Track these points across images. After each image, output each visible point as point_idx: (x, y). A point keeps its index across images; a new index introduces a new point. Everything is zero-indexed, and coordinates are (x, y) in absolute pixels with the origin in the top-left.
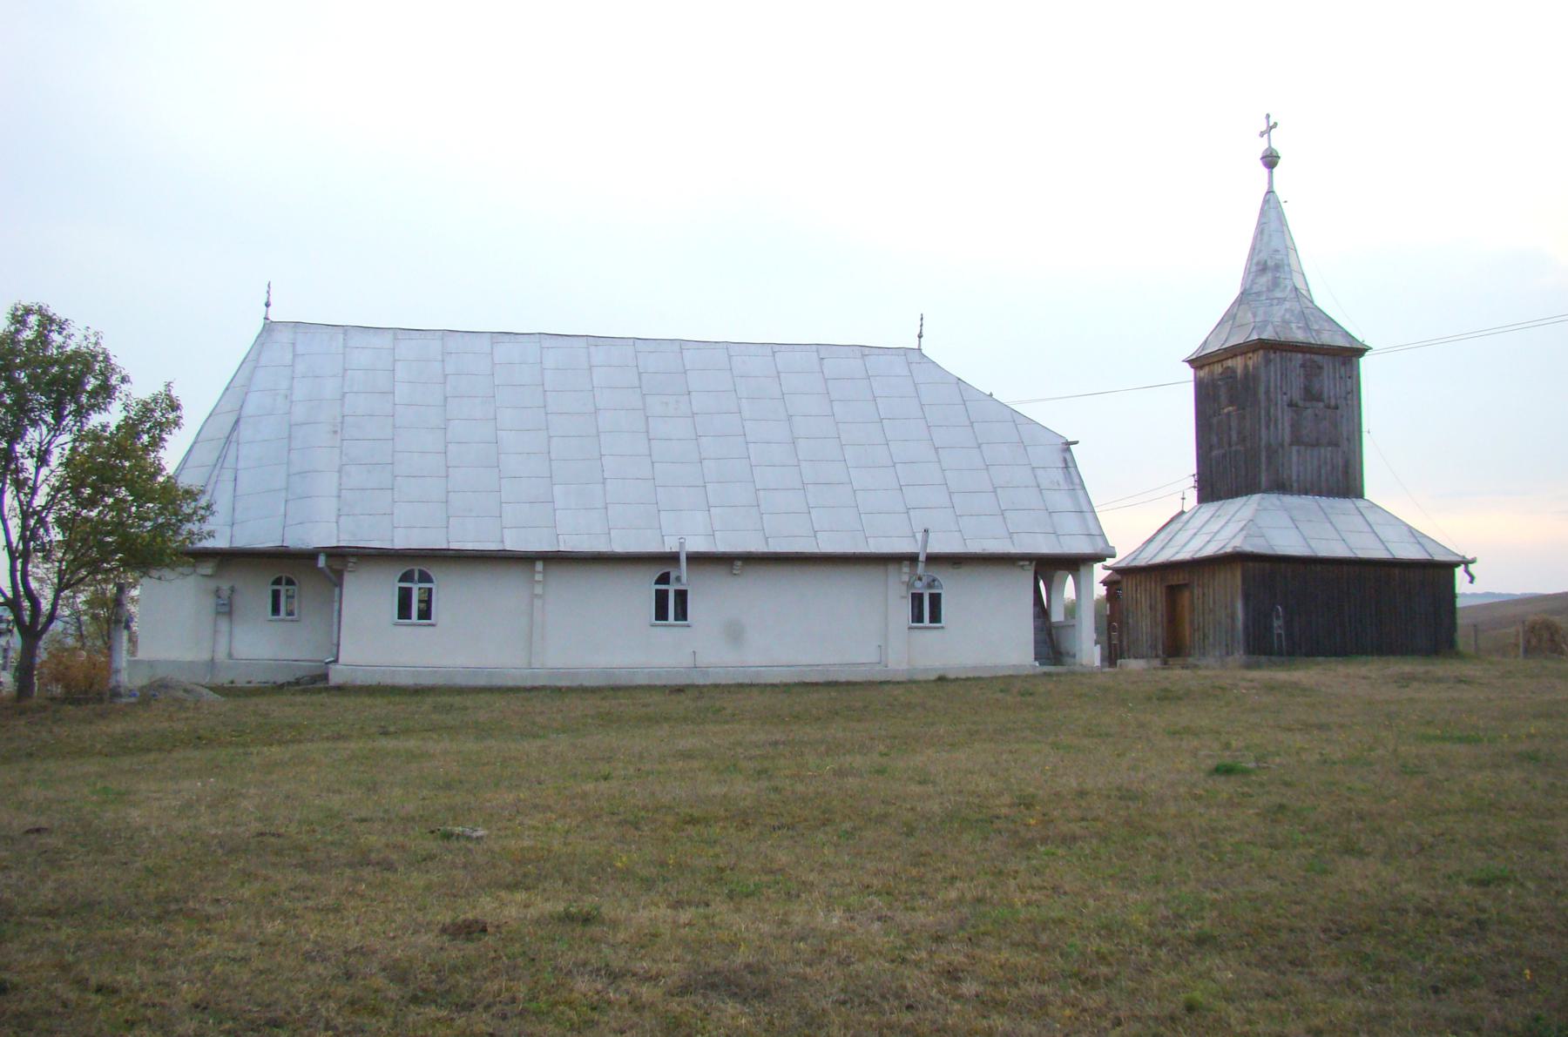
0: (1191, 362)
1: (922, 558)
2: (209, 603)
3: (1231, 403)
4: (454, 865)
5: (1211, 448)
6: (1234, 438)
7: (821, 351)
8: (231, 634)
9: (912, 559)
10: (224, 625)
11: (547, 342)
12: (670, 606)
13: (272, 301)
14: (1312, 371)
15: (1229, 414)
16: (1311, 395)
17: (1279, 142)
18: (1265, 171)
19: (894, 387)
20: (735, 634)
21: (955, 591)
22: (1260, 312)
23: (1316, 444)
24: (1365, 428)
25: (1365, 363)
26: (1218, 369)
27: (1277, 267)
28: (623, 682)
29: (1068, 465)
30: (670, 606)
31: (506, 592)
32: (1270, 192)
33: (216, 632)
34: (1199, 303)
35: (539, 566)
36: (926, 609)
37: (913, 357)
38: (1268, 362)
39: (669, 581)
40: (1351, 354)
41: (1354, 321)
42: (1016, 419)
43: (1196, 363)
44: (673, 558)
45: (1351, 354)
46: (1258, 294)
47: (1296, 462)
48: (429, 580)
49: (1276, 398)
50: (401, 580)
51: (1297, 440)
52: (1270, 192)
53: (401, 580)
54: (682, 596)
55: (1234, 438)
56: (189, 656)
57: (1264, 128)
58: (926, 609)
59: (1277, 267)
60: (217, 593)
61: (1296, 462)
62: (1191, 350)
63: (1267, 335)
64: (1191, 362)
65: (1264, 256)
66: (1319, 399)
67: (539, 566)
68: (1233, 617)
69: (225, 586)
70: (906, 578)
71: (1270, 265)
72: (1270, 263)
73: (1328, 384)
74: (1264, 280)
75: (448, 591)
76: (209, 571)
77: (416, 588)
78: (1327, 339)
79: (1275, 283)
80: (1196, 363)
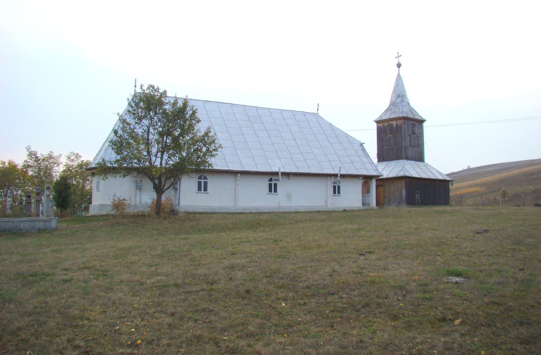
1: (339, 175)
2: (134, 185)
3: (391, 134)
5: (383, 147)
6: (392, 143)
7: (270, 110)
8: (141, 196)
9: (336, 175)
10: (138, 193)
11: (220, 105)
12: (273, 188)
14: (414, 125)
15: (390, 137)
16: (414, 133)
17: (401, 60)
18: (398, 68)
19: (309, 124)
20: (289, 197)
21: (345, 186)
22: (400, 108)
23: (414, 147)
24: (425, 142)
25: (424, 124)
26: (386, 124)
27: (403, 96)
28: (261, 211)
29: (364, 150)
30: (273, 188)
31: (228, 183)
32: (399, 74)
33: (136, 195)
34: (379, 106)
35: (239, 175)
36: (336, 190)
37: (316, 115)
38: (404, 123)
39: (273, 180)
40: (422, 121)
41: (422, 113)
42: (347, 136)
43: (378, 122)
44: (276, 174)
45: (422, 121)
46: (398, 103)
47: (411, 152)
49: (400, 134)
51: (410, 146)
52: (399, 74)
54: (275, 185)
55: (392, 143)
57: (397, 56)
58: (336, 190)
59: (403, 96)
60: (136, 182)
61: (411, 152)
62: (377, 117)
63: (404, 115)
64: (376, 122)
65: (399, 92)
66: (415, 134)
67: (239, 175)
68: (401, 194)
69: (138, 180)
70: (333, 181)
71: (399, 96)
72: (401, 95)
73: (416, 130)
74: (399, 100)
75: (283, 186)
76: (135, 175)
77: (203, 181)
79: (402, 101)
80: (378, 122)
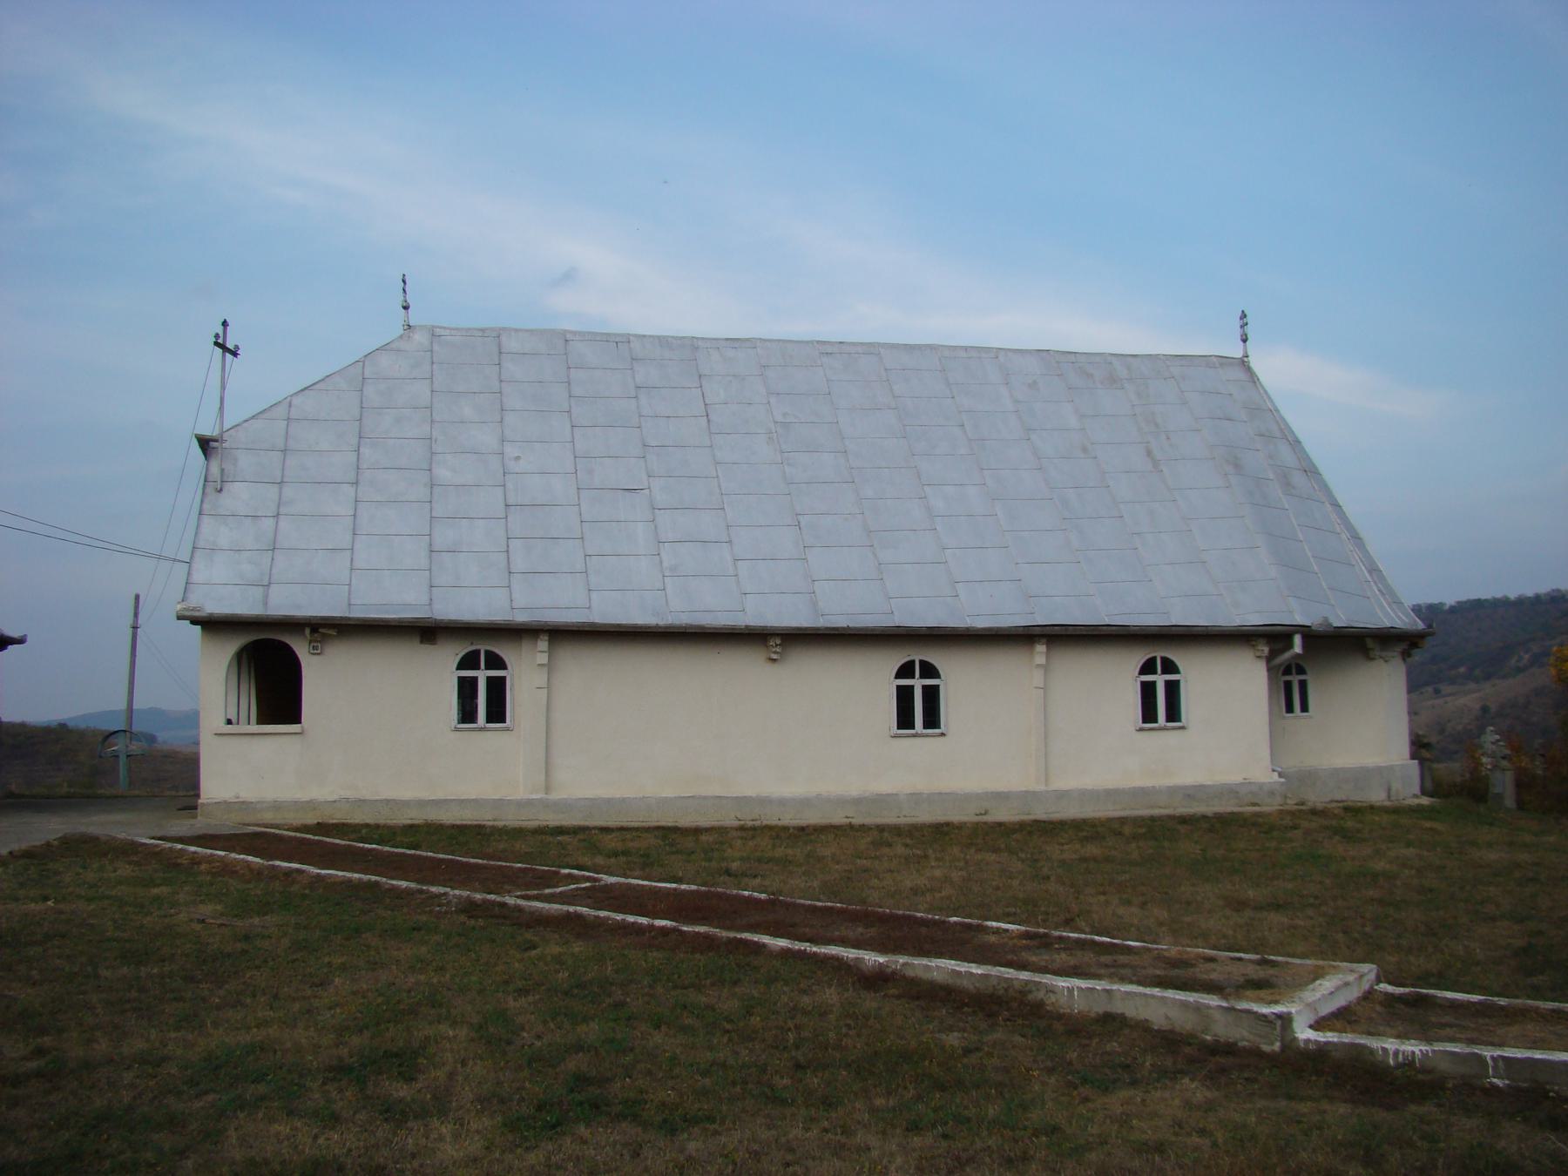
36: (918, 709)
53: (899, 675)
67: (543, 644)
77: (1160, 680)
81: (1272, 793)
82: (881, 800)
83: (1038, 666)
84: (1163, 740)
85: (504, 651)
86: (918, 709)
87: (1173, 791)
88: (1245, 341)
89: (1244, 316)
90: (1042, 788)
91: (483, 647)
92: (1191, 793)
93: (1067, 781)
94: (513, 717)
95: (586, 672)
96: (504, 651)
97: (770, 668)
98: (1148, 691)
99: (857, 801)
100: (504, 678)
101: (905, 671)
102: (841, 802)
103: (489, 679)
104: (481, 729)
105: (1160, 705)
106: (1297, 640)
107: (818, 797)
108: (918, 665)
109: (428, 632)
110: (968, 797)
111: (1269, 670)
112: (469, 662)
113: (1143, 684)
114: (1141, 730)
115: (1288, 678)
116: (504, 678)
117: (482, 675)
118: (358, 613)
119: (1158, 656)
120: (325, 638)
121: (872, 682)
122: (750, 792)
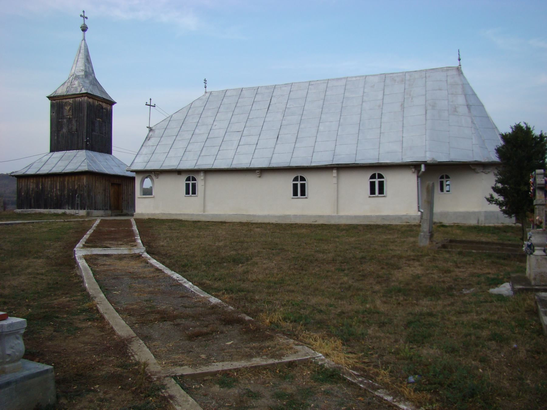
0: (49, 98)
4: (279, 309)
13: (461, 57)
21: (392, 181)
26: (96, 103)
36: (300, 190)
40: (112, 103)
45: (112, 103)
48: (383, 177)
50: (294, 180)
53: (294, 180)
56: (476, 210)
62: (50, 93)
64: (49, 98)
67: (202, 174)
77: (377, 181)
78: (97, 93)
81: (415, 219)
82: (285, 217)
83: (334, 177)
84: (378, 200)
85: (305, 175)
86: (300, 190)
87: (378, 217)
88: (205, 87)
89: (205, 80)
90: (335, 214)
91: (377, 172)
92: (384, 218)
93: (341, 213)
94: (386, 192)
95: (214, 182)
96: (305, 175)
97: (259, 179)
98: (187, 186)
99: (279, 217)
100: (383, 182)
101: (296, 179)
102: (275, 217)
103: (301, 184)
104: (377, 197)
105: (377, 189)
106: (423, 167)
107: (269, 215)
108: (299, 177)
109: (179, 172)
110: (311, 217)
111: (418, 177)
112: (188, 179)
113: (371, 182)
114: (370, 197)
115: (442, 180)
116: (383, 182)
117: (191, 182)
118: (313, 164)
119: (376, 175)
120: (158, 175)
121: (286, 183)
122: (251, 213)
